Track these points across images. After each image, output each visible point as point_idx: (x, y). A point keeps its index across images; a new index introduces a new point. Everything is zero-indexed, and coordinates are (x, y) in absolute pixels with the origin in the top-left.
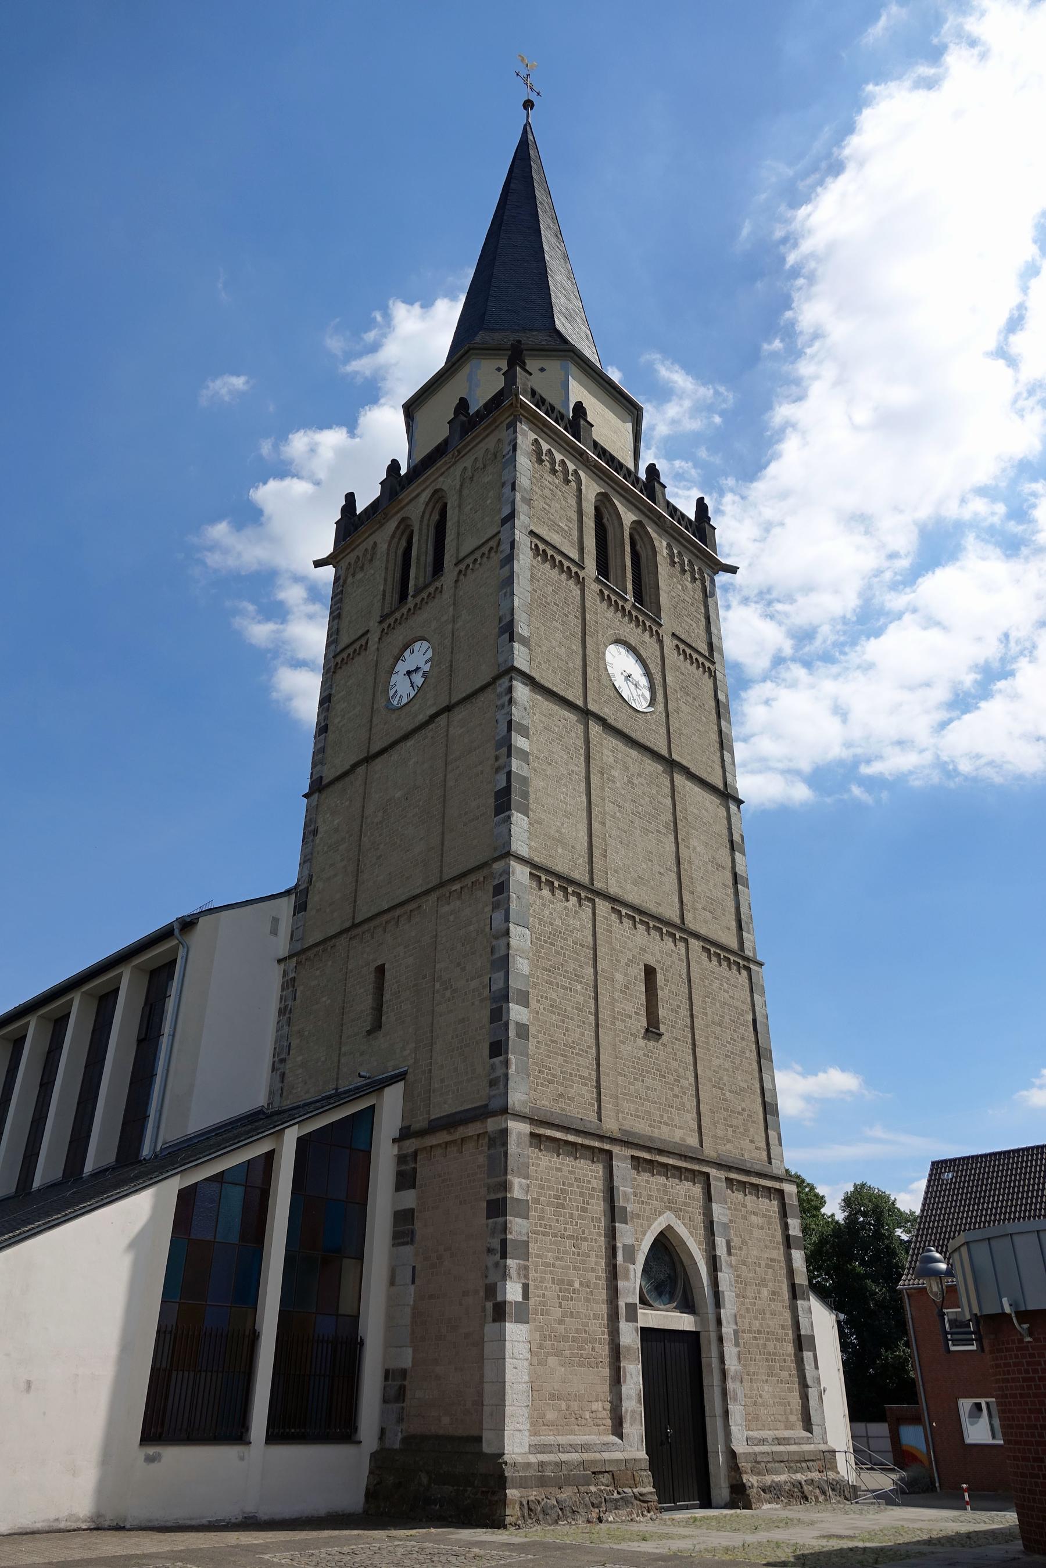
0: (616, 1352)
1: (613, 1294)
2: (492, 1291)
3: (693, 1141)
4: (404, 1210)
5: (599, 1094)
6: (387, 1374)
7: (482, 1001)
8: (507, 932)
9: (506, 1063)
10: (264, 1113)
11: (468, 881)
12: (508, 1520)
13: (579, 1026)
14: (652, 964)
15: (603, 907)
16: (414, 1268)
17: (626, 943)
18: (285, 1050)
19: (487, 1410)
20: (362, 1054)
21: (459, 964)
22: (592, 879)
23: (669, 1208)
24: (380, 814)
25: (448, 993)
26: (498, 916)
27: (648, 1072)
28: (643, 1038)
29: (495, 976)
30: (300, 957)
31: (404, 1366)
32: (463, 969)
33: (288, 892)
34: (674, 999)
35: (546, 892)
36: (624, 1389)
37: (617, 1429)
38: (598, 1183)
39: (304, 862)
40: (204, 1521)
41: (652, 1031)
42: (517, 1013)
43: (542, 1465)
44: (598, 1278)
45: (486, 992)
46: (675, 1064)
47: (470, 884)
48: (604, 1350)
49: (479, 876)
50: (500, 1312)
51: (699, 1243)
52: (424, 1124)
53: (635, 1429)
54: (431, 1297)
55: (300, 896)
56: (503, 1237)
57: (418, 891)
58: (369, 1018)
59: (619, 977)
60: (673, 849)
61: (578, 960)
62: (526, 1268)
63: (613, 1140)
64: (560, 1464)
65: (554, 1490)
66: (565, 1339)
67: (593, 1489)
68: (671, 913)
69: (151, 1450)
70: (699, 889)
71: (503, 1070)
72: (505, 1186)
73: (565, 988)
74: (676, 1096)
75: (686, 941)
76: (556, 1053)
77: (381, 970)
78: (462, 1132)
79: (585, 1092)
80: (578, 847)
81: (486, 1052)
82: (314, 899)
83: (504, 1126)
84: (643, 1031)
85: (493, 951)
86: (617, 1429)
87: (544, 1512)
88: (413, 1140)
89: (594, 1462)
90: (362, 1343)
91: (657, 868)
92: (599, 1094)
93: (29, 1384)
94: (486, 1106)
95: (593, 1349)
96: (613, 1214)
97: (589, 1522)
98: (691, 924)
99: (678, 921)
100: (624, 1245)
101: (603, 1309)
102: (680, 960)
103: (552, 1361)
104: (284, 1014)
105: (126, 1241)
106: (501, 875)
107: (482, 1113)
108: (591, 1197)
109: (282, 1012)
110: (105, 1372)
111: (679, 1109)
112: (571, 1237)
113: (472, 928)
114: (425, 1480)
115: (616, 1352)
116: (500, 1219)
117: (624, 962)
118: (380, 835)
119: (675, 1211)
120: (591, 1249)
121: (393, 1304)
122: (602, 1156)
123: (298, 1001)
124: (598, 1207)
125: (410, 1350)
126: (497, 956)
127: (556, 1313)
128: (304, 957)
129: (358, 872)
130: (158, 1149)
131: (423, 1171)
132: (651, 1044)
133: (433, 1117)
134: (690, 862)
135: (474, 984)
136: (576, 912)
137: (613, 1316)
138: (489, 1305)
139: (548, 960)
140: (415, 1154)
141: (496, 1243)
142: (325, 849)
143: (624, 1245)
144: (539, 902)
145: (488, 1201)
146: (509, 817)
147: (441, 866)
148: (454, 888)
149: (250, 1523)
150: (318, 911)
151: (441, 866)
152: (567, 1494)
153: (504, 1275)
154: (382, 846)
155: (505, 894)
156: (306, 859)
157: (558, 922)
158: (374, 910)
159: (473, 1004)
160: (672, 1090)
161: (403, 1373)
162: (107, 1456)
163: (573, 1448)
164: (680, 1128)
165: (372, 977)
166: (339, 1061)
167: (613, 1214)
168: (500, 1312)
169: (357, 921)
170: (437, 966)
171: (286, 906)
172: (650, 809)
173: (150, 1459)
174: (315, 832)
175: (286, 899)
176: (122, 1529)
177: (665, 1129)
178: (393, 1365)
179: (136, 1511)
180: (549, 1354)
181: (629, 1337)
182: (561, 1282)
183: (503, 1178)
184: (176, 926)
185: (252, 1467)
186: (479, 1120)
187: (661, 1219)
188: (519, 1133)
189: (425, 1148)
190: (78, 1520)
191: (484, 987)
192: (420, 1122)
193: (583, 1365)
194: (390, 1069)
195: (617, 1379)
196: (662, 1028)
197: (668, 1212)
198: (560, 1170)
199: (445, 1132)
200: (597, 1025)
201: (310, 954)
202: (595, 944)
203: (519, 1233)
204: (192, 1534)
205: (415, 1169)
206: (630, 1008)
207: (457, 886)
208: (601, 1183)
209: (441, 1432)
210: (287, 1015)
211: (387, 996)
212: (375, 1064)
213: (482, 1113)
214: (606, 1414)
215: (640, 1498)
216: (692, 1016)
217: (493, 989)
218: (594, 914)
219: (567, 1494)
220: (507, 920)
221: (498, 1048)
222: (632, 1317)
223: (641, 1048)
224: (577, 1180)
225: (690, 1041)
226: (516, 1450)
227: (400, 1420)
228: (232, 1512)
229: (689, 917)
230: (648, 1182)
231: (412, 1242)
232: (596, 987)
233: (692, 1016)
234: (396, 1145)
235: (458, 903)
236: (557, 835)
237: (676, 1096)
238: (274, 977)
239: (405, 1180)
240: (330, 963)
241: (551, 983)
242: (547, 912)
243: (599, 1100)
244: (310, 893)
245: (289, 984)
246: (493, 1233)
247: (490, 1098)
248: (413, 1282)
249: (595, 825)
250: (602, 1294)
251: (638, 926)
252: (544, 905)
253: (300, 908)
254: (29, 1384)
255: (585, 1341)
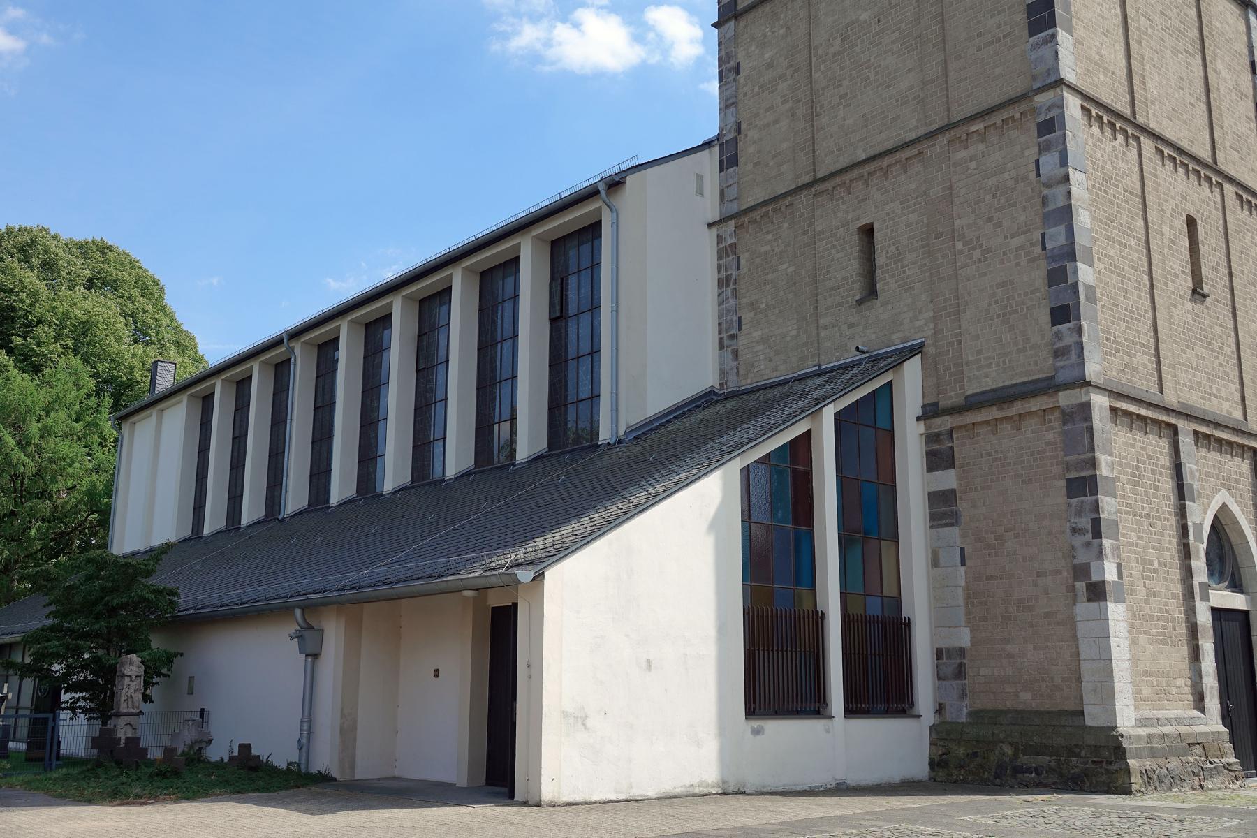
0: (1193, 631)
1: (1188, 572)
2: (1081, 571)
3: (1238, 415)
4: (943, 492)
5: (1159, 363)
6: (939, 653)
7: (1031, 261)
8: (1066, 179)
9: (1079, 330)
10: (715, 393)
11: (997, 119)
12: (1134, 787)
13: (1136, 288)
14: (1193, 213)
15: (1148, 144)
16: (962, 550)
17: (1169, 190)
18: (735, 325)
19: (1087, 687)
20: (851, 326)
21: (990, 219)
22: (1134, 113)
23: (1223, 485)
24: (838, 41)
25: (977, 254)
26: (1049, 163)
27: (1197, 338)
28: (1191, 300)
29: (1050, 232)
30: (737, 221)
31: (963, 645)
32: (999, 225)
33: (707, 144)
34: (1214, 255)
35: (1095, 130)
36: (1203, 665)
37: (1199, 701)
38: (1165, 460)
39: (727, 107)
40: (806, 787)
41: (1198, 293)
42: (1085, 273)
43: (1150, 736)
44: (1172, 557)
45: (1038, 250)
46: (1218, 330)
47: (999, 123)
48: (1182, 629)
49: (1015, 112)
50: (1097, 592)
51: (1250, 522)
52: (961, 401)
53: (1213, 703)
54: (990, 578)
55: (726, 148)
56: (1095, 516)
57: (913, 136)
58: (857, 286)
59: (1166, 229)
60: (1201, 73)
61: (1130, 211)
62: (1118, 547)
63: (1178, 413)
64: (1163, 736)
65: (1162, 760)
66: (1151, 618)
67: (1191, 759)
68: (1204, 153)
69: (756, 724)
70: (1226, 124)
71: (1076, 338)
72: (1093, 463)
73: (1120, 243)
74: (1221, 365)
75: (1220, 186)
76: (1119, 319)
77: (868, 232)
78: (1018, 407)
79: (1145, 361)
80: (1118, 72)
81: (1045, 317)
82: (747, 151)
83: (1084, 399)
84: (1190, 292)
85: (1044, 201)
86: (1199, 701)
87: (1160, 781)
88: (948, 417)
89: (1188, 734)
90: (908, 624)
91: (1189, 99)
92: (1159, 363)
93: (649, 662)
94: (1053, 377)
95: (1173, 628)
96: (1181, 491)
97: (1193, 789)
98: (1223, 165)
99: (1210, 160)
100: (1194, 524)
101: (1178, 588)
102: (1216, 209)
103: (1143, 639)
104: (728, 285)
105: (705, 525)
106: (1049, 109)
107: (1049, 386)
108: (1161, 474)
109: (723, 283)
110: (709, 651)
111: (1224, 379)
112: (1147, 516)
113: (1006, 176)
114: (1009, 751)
115: (1193, 631)
116: (1089, 498)
117: (1169, 212)
118: (841, 69)
119: (1229, 488)
120: (1164, 527)
121: (938, 589)
122: (1165, 432)
123: (744, 270)
124: (1167, 484)
125: (967, 630)
126: (1051, 207)
127: (1142, 592)
128: (745, 219)
129: (813, 116)
130: (622, 432)
131: (962, 448)
132: (1198, 306)
133: (969, 393)
134: (1218, 90)
135: (1015, 242)
136: (1124, 153)
137: (1189, 594)
138: (1081, 586)
139: (1105, 211)
140: (950, 433)
141: (1085, 522)
142: (756, 89)
143: (1194, 524)
144: (1090, 142)
145: (1068, 480)
146: (1054, 36)
147: (947, 103)
148: (973, 128)
149: (841, 790)
150: (755, 164)
151: (947, 103)
152: (1173, 763)
153: (1100, 555)
154: (846, 83)
155: (1058, 133)
156: (727, 103)
157: (1108, 166)
158: (844, 161)
159: (1018, 265)
160: (1218, 358)
161: (961, 652)
162: (723, 730)
163: (1168, 722)
164: (1227, 400)
165: (855, 239)
166: (818, 335)
167: (1181, 491)
168: (1097, 592)
169: (819, 175)
170: (957, 223)
171: (710, 160)
172: (1178, 24)
173: (756, 732)
174: (737, 69)
175: (706, 153)
176: (744, 793)
177: (1215, 401)
178: (943, 644)
179: (753, 780)
180: (1139, 633)
181: (1204, 618)
182: (1144, 562)
183: (1090, 455)
184: (602, 187)
185: (835, 738)
186: (1050, 393)
187: (1217, 497)
188: (1101, 407)
189: (965, 426)
190: (708, 786)
191: (1032, 245)
192: (952, 397)
193: (1166, 644)
194: (898, 341)
195: (1195, 656)
196: (1206, 290)
197: (1223, 490)
198: (1133, 446)
199: (995, 408)
200: (1152, 286)
201: (755, 215)
202: (1143, 191)
203: (1110, 512)
204: (869, 799)
205: (952, 448)
206: (1178, 269)
207: (978, 126)
208: (1167, 459)
209: (1021, 707)
210: (732, 286)
211: (880, 260)
212: (873, 336)
213: (1049, 386)
214: (1187, 690)
215: (1228, 767)
216: (1230, 274)
217: (1048, 246)
218: (1140, 155)
219: (1173, 763)
220: (1064, 162)
221: (1064, 313)
222: (1205, 598)
223: (1189, 312)
224: (1149, 456)
225: (1229, 303)
226: (1126, 724)
227: (963, 696)
228: (826, 780)
229: (1221, 157)
230: (1205, 458)
231: (957, 523)
232: (1148, 242)
233: (1230, 274)
234: (922, 425)
235: (981, 147)
236: (1098, 58)
237: (1221, 365)
238: (707, 245)
239: (937, 459)
240: (786, 225)
241: (1108, 238)
242: (1098, 154)
243: (1159, 371)
244: (740, 144)
245: (726, 252)
246: (1079, 512)
247: (1057, 370)
248: (963, 563)
249: (1133, 45)
250: (1176, 574)
251: (1179, 169)
252: (1095, 145)
253: (729, 161)
254: (649, 662)
255: (1167, 620)
